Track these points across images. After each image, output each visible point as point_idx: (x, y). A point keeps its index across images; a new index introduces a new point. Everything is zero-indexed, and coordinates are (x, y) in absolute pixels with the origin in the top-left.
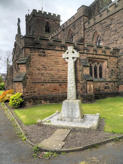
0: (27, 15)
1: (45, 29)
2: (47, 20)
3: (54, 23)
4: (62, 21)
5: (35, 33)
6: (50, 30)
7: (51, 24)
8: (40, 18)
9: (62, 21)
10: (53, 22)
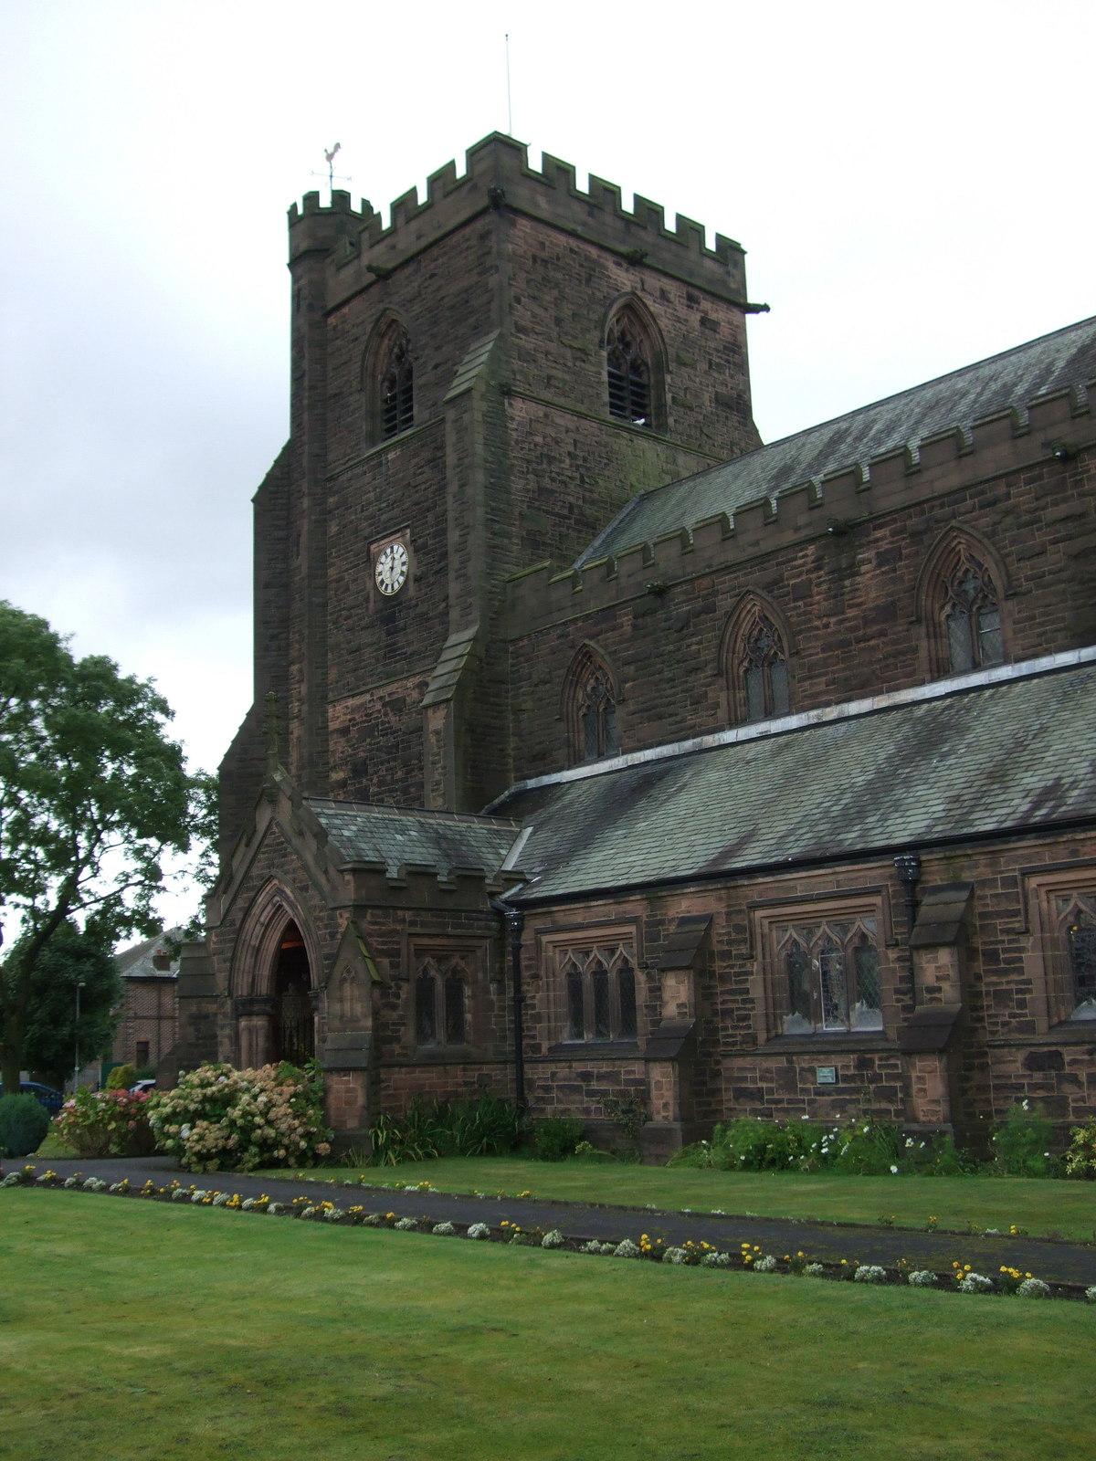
0: (325, 202)
1: (611, 375)
2: (624, 279)
3: (695, 318)
4: (766, 308)
5: (520, 410)
6: (661, 396)
7: (664, 323)
8: (562, 239)
9: (766, 308)
10: (683, 312)
